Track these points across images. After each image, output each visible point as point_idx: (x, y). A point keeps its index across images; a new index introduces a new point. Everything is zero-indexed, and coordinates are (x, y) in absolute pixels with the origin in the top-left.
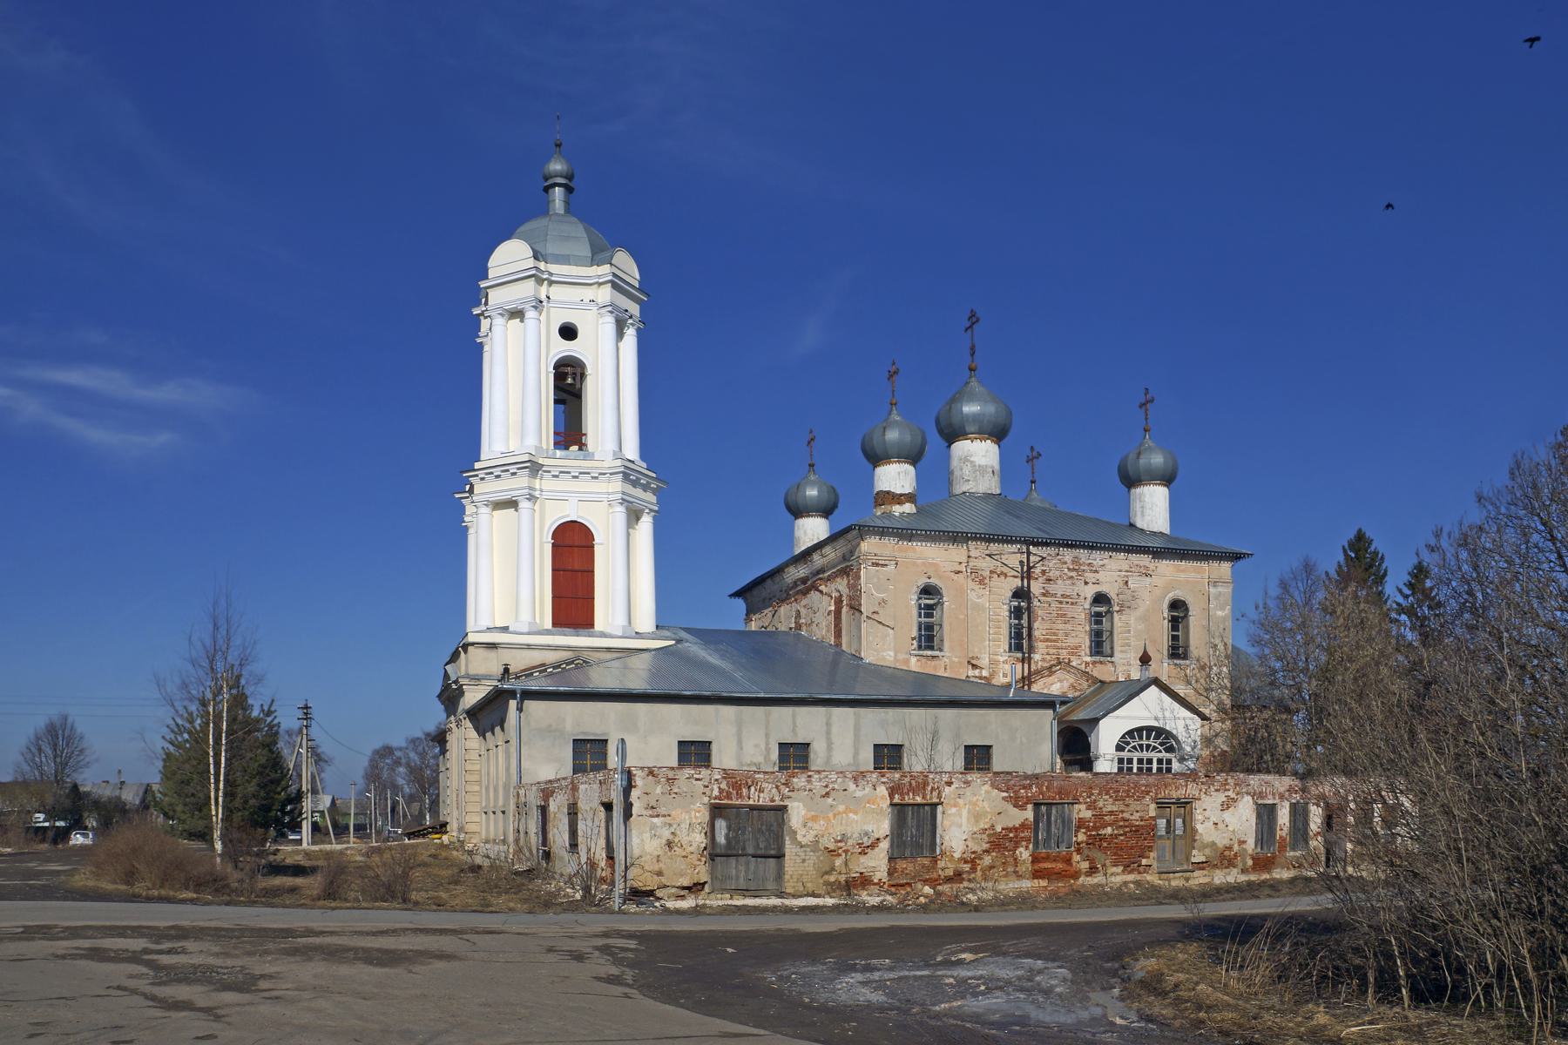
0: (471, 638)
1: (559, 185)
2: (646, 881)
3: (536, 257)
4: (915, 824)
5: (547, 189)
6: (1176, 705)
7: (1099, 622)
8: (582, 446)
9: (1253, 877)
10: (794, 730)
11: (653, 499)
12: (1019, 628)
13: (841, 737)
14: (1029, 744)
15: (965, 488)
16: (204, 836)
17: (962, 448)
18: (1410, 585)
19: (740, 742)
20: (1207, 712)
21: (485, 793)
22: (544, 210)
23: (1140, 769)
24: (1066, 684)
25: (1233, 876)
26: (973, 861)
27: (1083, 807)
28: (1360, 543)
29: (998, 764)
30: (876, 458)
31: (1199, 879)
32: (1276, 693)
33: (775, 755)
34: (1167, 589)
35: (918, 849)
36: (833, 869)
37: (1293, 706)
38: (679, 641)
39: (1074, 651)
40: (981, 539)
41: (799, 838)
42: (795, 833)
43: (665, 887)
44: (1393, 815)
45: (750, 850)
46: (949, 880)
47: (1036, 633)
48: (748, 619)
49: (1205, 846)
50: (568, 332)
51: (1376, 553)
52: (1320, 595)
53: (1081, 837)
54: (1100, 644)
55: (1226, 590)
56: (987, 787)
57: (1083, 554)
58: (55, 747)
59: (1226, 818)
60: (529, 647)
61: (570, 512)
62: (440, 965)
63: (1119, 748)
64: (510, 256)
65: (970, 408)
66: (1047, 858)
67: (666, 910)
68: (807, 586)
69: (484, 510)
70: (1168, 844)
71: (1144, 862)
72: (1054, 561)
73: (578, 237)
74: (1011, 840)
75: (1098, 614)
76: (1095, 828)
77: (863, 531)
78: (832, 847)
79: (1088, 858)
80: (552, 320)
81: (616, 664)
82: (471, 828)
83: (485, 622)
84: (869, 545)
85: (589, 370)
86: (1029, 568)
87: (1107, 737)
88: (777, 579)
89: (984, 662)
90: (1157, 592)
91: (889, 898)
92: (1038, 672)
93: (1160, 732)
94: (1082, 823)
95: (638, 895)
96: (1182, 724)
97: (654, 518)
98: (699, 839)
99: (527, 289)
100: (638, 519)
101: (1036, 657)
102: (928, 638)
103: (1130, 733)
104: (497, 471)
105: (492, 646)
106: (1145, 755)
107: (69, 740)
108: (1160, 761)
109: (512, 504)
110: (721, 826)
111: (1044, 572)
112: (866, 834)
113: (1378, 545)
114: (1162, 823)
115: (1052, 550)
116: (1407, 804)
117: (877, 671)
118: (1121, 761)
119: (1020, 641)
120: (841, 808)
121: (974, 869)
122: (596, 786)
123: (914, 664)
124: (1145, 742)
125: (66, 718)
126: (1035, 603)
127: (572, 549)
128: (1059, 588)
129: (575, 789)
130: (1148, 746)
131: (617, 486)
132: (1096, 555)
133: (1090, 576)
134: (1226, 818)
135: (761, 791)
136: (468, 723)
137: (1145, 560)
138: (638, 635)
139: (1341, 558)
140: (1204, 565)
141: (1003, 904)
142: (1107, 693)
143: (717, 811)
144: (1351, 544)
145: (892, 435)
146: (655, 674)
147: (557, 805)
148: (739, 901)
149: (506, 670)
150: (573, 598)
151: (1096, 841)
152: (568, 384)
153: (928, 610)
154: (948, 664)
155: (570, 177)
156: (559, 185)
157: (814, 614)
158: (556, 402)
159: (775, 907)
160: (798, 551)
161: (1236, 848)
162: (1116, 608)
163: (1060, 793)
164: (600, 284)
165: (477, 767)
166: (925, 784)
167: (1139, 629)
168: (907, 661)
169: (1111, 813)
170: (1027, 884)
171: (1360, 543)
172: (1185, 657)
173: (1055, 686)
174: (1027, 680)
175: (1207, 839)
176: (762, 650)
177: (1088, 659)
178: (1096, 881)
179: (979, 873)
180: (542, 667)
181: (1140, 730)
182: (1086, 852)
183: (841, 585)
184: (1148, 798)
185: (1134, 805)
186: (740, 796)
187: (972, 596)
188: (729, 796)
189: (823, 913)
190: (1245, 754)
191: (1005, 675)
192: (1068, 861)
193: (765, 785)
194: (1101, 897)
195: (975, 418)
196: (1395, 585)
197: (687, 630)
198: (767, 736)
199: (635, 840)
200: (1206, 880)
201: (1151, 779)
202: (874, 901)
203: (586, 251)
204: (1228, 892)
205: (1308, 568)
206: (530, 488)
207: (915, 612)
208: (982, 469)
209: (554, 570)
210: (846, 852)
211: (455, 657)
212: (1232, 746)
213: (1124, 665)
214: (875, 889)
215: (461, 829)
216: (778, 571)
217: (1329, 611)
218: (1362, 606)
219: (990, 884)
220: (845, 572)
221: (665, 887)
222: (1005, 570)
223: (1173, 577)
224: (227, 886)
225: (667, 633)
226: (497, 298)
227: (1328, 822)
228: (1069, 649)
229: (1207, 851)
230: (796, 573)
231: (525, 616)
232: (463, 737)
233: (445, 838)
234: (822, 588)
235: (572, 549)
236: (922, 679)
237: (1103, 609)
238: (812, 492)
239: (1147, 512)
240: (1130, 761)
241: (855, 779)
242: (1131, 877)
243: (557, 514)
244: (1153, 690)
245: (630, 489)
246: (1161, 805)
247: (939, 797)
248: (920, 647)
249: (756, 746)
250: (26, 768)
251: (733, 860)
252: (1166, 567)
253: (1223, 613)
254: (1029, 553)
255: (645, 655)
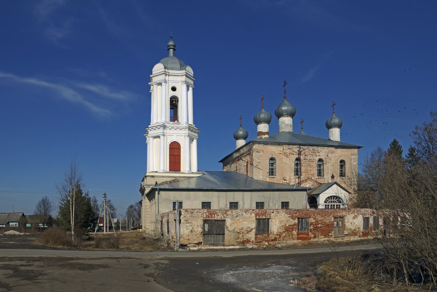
0: (147, 174)
1: (172, 48)
2: (185, 242)
3: (165, 68)
4: (263, 225)
5: (168, 50)
6: (342, 190)
7: (320, 167)
8: (178, 120)
9: (362, 238)
10: (234, 199)
11: (197, 135)
12: (297, 169)
13: (247, 200)
14: (299, 201)
15: (283, 130)
16: (69, 229)
17: (282, 119)
18: (409, 154)
19: (219, 202)
20: (350, 191)
21: (151, 216)
22: (167, 55)
23: (337, 208)
24: (310, 184)
25: (356, 238)
26: (280, 235)
27: (312, 219)
28: (395, 143)
29: (290, 207)
30: (258, 122)
31: (346, 239)
32: (370, 185)
33: (228, 206)
34: (339, 157)
35: (264, 232)
36: (239, 238)
37: (375, 189)
38: (203, 174)
39: (313, 175)
40: (287, 144)
41: (229, 229)
42: (228, 227)
43: (190, 243)
44: (404, 219)
45: (215, 233)
46: (273, 240)
47: (302, 170)
48: (223, 168)
49: (348, 229)
50: (174, 89)
51: (399, 146)
52: (383, 158)
53: (312, 227)
54: (320, 173)
55: (356, 157)
56: (284, 213)
57: (315, 148)
58: (44, 206)
59: (354, 221)
60: (163, 177)
61: (174, 139)
62: (101, 270)
63: (325, 202)
64: (158, 68)
65: (284, 108)
66: (302, 234)
67: (190, 251)
68: (239, 158)
69: (151, 139)
70: (337, 229)
71: (330, 234)
72: (307, 150)
73: (176, 62)
74: (291, 229)
75: (320, 165)
76: (316, 225)
77: (254, 143)
78: (239, 231)
79: (313, 234)
80: (170, 86)
81: (186, 181)
82: (147, 227)
83: (151, 170)
84: (256, 147)
85: (179, 99)
86: (300, 152)
87: (322, 199)
88: (231, 157)
89: (288, 179)
90: (336, 158)
91: (255, 246)
92: (303, 181)
93: (337, 197)
94: (312, 224)
95: (183, 246)
96: (343, 194)
97: (197, 140)
98: (200, 230)
99: (162, 77)
100: (193, 141)
101: (302, 177)
102: (272, 172)
103: (328, 198)
104: (154, 128)
105: (153, 177)
106: (333, 204)
107: (48, 203)
108: (337, 205)
109: (158, 137)
110: (206, 226)
111: (304, 153)
112: (249, 227)
113: (400, 143)
114: (335, 223)
115: (307, 147)
116: (407, 216)
117: (258, 182)
118: (326, 206)
119: (298, 172)
120: (241, 220)
121: (280, 237)
122: (173, 215)
123: (268, 180)
124: (332, 200)
125: (47, 197)
126: (302, 162)
127: (175, 148)
128: (309, 157)
129: (168, 216)
130: (334, 201)
131: (187, 131)
132: (319, 148)
133: (317, 154)
134: (354, 221)
135: (218, 215)
136: (146, 198)
137: (333, 149)
138: (193, 173)
139: (389, 147)
140: (350, 150)
141: (288, 247)
142: (322, 187)
143: (205, 221)
144: (392, 143)
145: (262, 116)
146: (197, 184)
147: (165, 220)
148: (211, 247)
149: (156, 183)
150: (175, 163)
151: (316, 228)
152: (174, 103)
153: (272, 164)
154: (277, 179)
155: (174, 46)
156: (172, 48)
157: (240, 167)
158: (170, 108)
159: (221, 249)
160: (237, 149)
161: (357, 230)
162: (325, 163)
163: (305, 215)
164: (182, 76)
165: (149, 210)
166: (266, 213)
167: (332, 167)
168: (266, 179)
169: (320, 220)
170: (296, 241)
171: (395, 143)
172: (344, 176)
173: (307, 185)
174: (299, 183)
175: (349, 227)
176: (227, 177)
177: (317, 177)
178: (316, 240)
179: (281, 238)
180: (166, 182)
181: (331, 197)
182: (313, 232)
183: (248, 158)
184: (331, 216)
185: (327, 218)
186: (212, 217)
187: (284, 160)
188: (209, 217)
189: (235, 251)
190: (362, 202)
191: (293, 182)
192: (308, 234)
193: (219, 214)
194: (318, 245)
195: (286, 111)
196: (405, 153)
197: (206, 171)
198: (226, 200)
199: (182, 230)
200: (348, 239)
201: (332, 210)
202: (251, 247)
203: (179, 66)
204: (354, 243)
205: (380, 150)
206: (163, 132)
207: (268, 165)
208: (287, 125)
209: (170, 155)
210: (243, 233)
211: (143, 180)
212: (358, 201)
213: (327, 179)
214: (251, 243)
215: (145, 227)
216: (231, 155)
217: (385, 162)
218: (395, 160)
219: (285, 242)
220: (249, 154)
221: (190, 243)
222: (294, 153)
223: (341, 153)
224: (72, 244)
225: (201, 172)
226: (155, 80)
227: (384, 222)
228: (312, 176)
229: (349, 231)
230: (236, 155)
231: (162, 168)
232: (146, 202)
233: (141, 230)
234: (243, 159)
235: (175, 148)
236: (270, 184)
237: (321, 163)
238: (241, 133)
239: (334, 135)
240: (328, 206)
241: (245, 212)
242: (326, 239)
243: (170, 140)
244: (335, 185)
245: (190, 132)
246: (335, 218)
247: (270, 216)
248: (270, 175)
249: (223, 203)
250: (37, 211)
251: (210, 236)
252: (339, 151)
253: (355, 163)
254: (300, 148)
255: (193, 178)
